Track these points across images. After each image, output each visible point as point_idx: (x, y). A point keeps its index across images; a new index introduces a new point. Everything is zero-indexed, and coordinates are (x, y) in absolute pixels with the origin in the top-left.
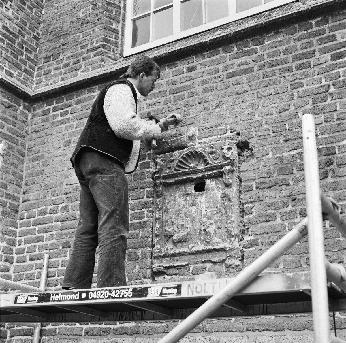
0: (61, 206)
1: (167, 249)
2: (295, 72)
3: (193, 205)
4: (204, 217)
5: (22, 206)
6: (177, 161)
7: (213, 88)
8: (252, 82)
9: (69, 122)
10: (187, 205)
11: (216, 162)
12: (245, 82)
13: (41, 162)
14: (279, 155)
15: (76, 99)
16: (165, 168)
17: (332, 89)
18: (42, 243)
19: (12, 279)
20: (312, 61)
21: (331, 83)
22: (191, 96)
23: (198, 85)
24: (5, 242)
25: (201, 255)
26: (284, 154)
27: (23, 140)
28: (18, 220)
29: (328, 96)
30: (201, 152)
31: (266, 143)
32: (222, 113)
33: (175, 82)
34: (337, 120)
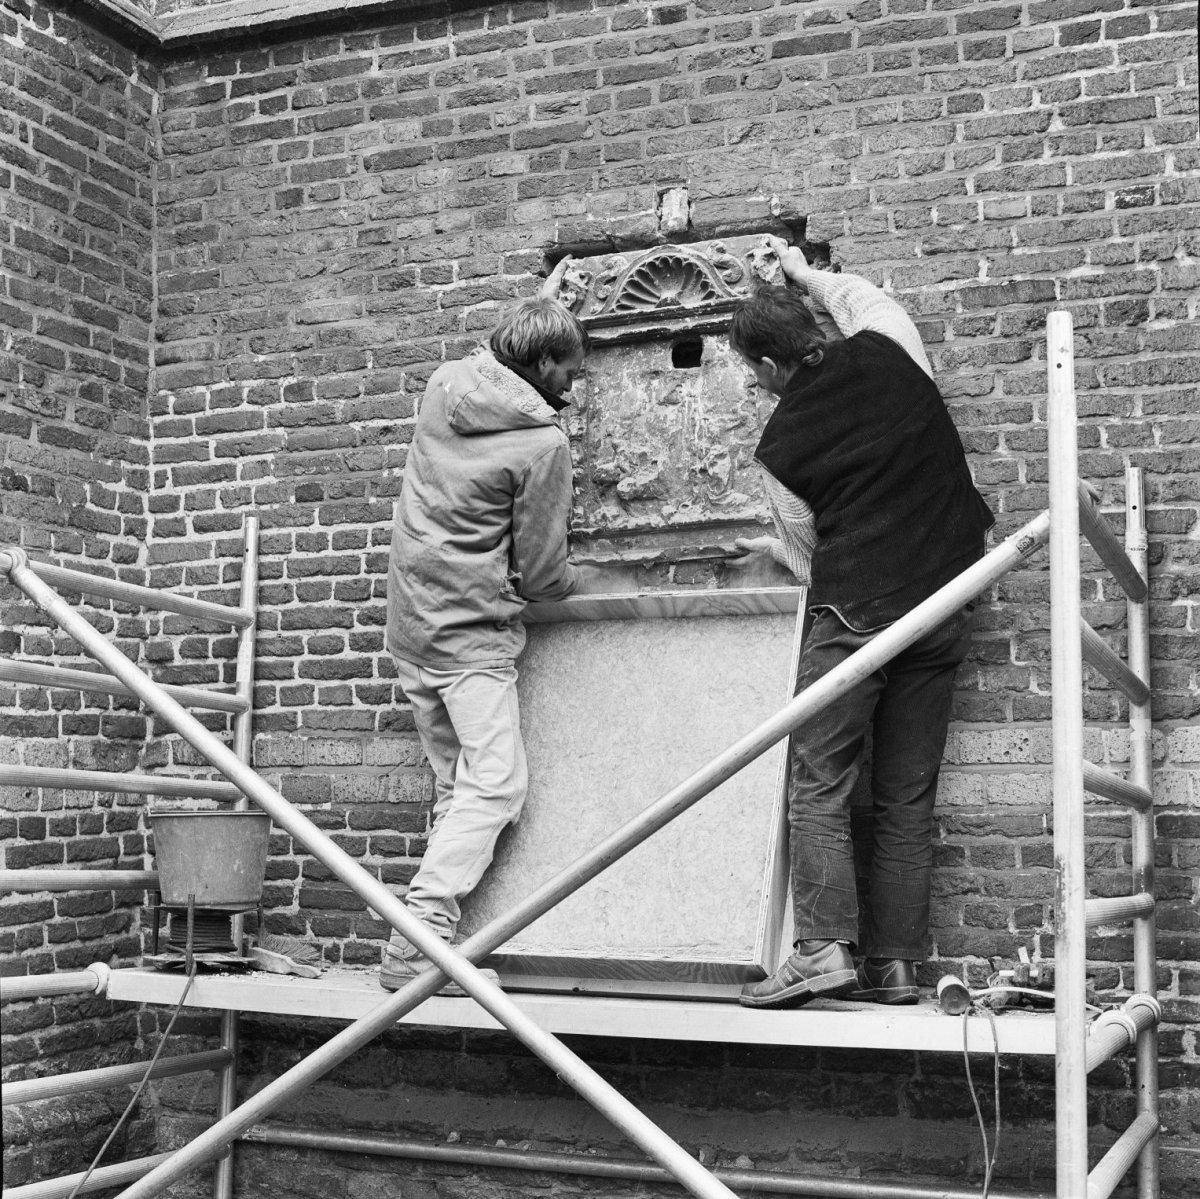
0: (285, 382)
1: (604, 517)
2: (964, 64)
3: (668, 402)
4: (700, 437)
5: (155, 373)
6: (624, 283)
7: (733, 81)
8: (843, 79)
9: (291, 135)
10: (654, 402)
11: (733, 292)
12: (823, 75)
13: (207, 247)
14: (909, 291)
15: (307, 63)
16: (591, 299)
17: (1057, 126)
18: (233, 483)
19: (147, 583)
20: (1011, 38)
21: (1056, 107)
22: (670, 99)
23: (691, 67)
24: (123, 482)
25: (693, 534)
26: (924, 288)
27: (144, 180)
28: (149, 417)
29: (1047, 143)
30: (692, 260)
31: (877, 255)
32: (760, 157)
33: (620, 50)
34: (1064, 211)
